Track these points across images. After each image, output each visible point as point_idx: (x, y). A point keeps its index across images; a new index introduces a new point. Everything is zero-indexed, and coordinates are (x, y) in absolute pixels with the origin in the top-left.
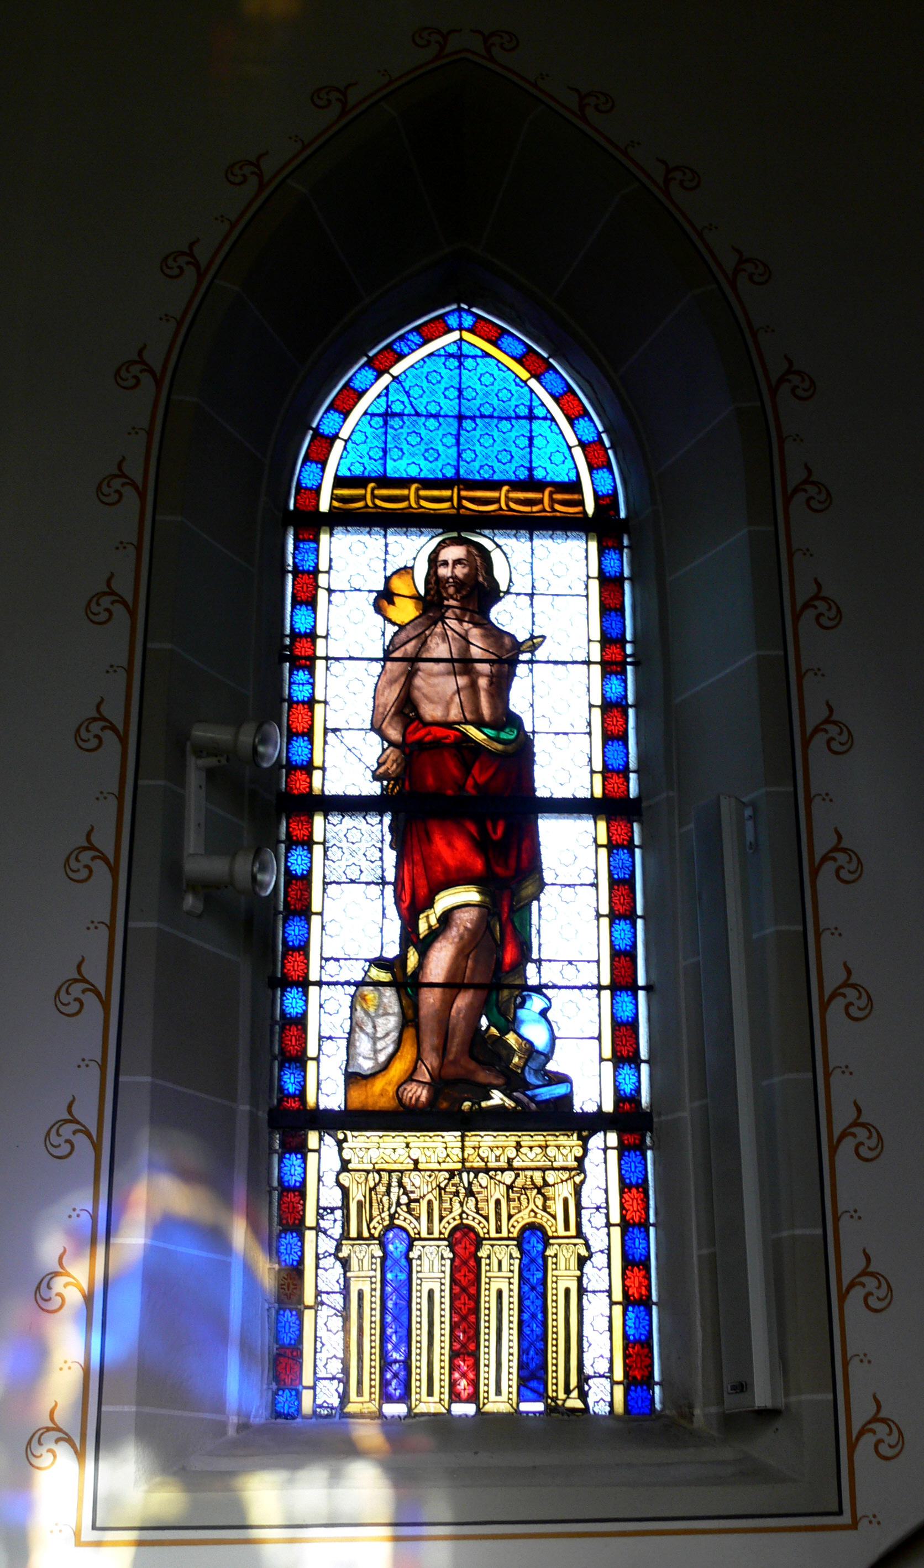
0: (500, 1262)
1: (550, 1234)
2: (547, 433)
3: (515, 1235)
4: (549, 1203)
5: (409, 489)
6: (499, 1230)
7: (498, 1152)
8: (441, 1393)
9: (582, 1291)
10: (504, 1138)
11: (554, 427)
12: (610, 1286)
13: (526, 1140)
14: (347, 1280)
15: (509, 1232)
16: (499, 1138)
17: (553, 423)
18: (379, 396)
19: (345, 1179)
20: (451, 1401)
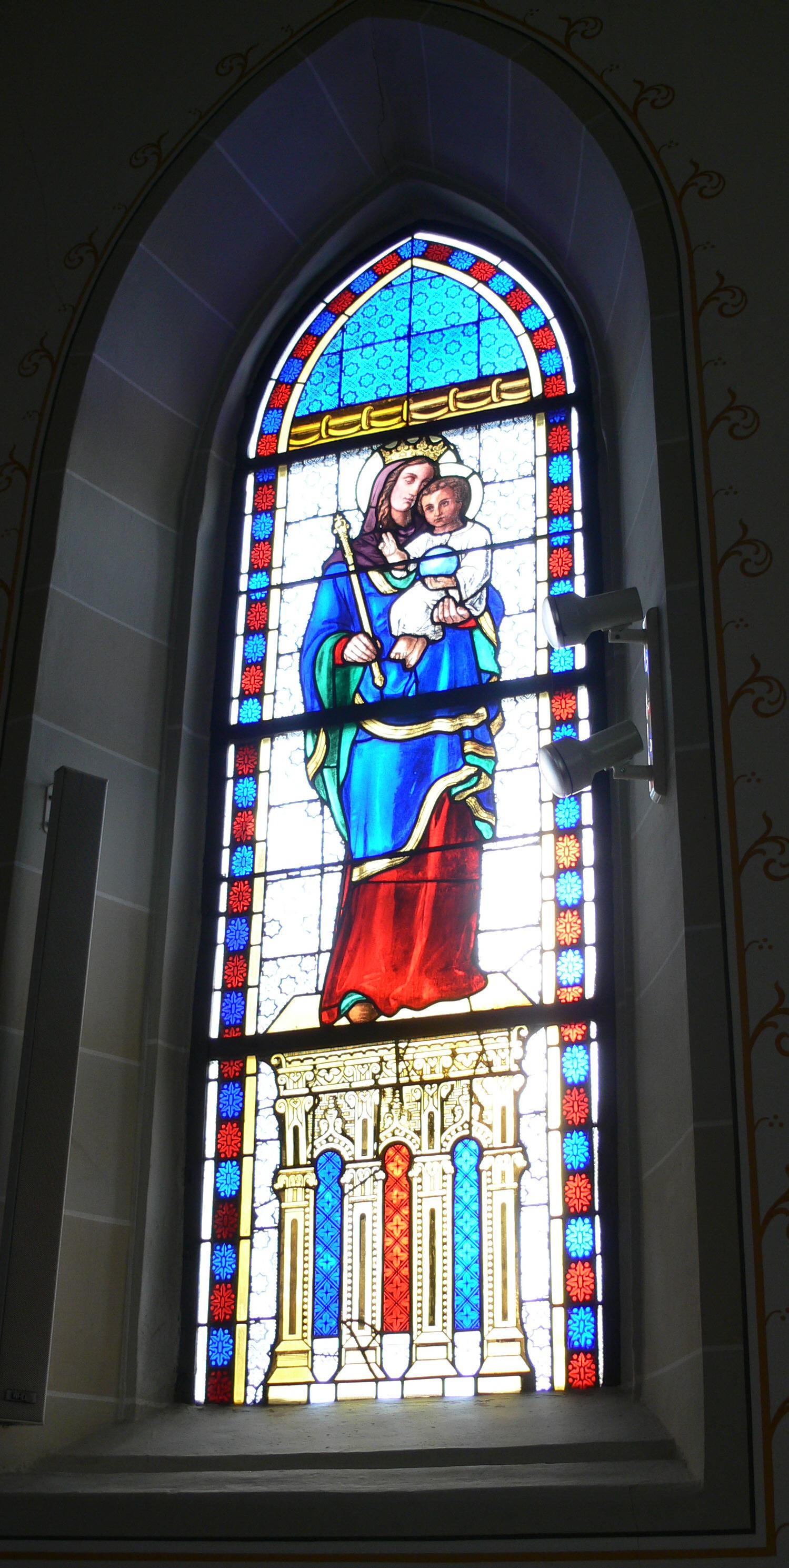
0: (503, 1174)
1: (414, 1153)
2: (497, 332)
3: (448, 1150)
4: (347, 1126)
5: (448, 395)
6: (364, 1152)
7: (432, 1063)
8: (304, 1331)
9: (518, 1205)
10: (361, 1055)
11: (502, 323)
12: (549, 1201)
13: (321, 1063)
14: (282, 1211)
15: (442, 1147)
16: (355, 1056)
17: (502, 320)
18: (335, 337)
19: (281, 1107)
20: (314, 1337)
